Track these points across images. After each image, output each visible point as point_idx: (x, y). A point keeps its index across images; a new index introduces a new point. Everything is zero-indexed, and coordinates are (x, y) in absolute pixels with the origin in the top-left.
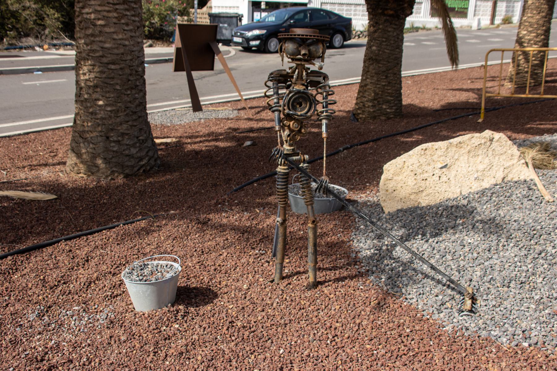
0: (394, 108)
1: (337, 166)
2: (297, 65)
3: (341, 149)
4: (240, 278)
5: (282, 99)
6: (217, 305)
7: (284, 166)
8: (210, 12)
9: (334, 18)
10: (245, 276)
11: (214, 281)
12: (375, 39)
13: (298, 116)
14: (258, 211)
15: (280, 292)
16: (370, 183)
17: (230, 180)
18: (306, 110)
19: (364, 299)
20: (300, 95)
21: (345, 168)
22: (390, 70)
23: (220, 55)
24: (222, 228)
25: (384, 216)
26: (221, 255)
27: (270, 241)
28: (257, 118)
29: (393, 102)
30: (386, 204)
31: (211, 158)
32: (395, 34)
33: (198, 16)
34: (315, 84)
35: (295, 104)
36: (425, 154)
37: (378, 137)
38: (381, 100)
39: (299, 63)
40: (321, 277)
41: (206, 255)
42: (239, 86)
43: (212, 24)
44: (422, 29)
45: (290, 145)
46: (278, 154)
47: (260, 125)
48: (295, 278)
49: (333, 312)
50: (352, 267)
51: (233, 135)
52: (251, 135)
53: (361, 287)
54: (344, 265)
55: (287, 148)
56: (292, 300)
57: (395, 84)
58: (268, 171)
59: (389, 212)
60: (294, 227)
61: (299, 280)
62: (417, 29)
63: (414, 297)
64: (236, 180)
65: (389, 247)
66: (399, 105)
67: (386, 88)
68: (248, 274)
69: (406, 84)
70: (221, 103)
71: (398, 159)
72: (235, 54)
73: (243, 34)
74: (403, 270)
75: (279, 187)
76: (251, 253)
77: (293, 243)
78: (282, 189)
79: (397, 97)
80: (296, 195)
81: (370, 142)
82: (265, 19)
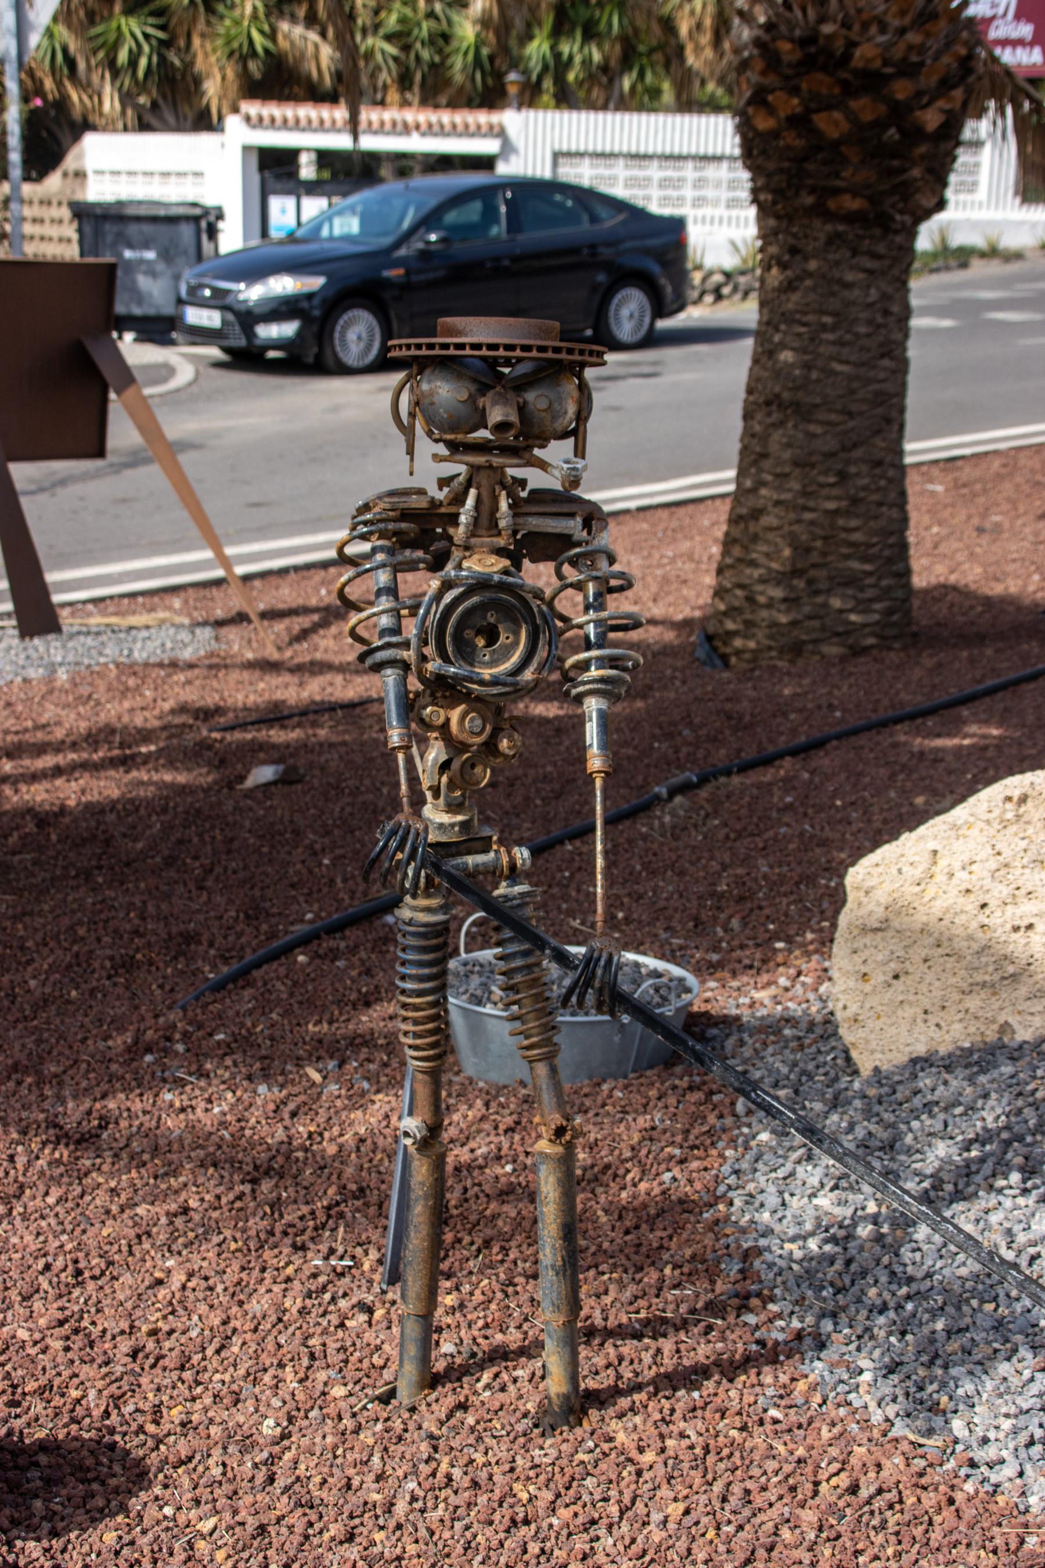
0: (877, 606)
1: (646, 866)
2: (474, 469)
3: (662, 790)
4: (247, 1390)
5: (413, 614)
6: (147, 1522)
7: (428, 896)
8: (79, 197)
9: (611, 221)
10: (267, 1378)
11: (129, 1408)
12: (788, 318)
13: (482, 683)
14: (317, 1077)
15: (425, 1448)
16: (789, 940)
17: (190, 938)
18: (515, 658)
19: (788, 1468)
20: (489, 595)
21: (682, 873)
22: (855, 445)
23: (130, 393)
24: (157, 1154)
25: (856, 1085)
26: (160, 1282)
27: (373, 1210)
28: (298, 660)
29: (869, 581)
30: (861, 1033)
31: (107, 843)
32: (874, 294)
33: (27, 212)
34: (551, 547)
35: (468, 633)
36: (1018, 817)
37: (816, 734)
38: (823, 573)
39: (480, 460)
40: (597, 1365)
41: (91, 1286)
42: (214, 521)
43: (90, 260)
44: (983, 255)
45: (452, 808)
46: (400, 847)
47: (314, 689)
48: (486, 1377)
49: (657, 1536)
50: (731, 1319)
51: (201, 737)
52: (277, 736)
53: (773, 1413)
54: (693, 1311)
55: (437, 817)
56: (475, 1484)
57: (880, 504)
58: (352, 894)
59: (877, 1070)
60: (475, 1138)
61: (503, 1389)
62: (963, 257)
63: (1005, 1453)
64: (219, 941)
65: (885, 1229)
66: (900, 594)
67: (841, 522)
68: (281, 1365)
69: (922, 496)
70: (143, 593)
71: (907, 839)
72: (196, 380)
73: (227, 292)
74: (949, 1333)
75: (409, 985)
76: (290, 1270)
77: (473, 1218)
78: (420, 994)
79: (889, 561)
80: (479, 1002)
81: (780, 756)
82: (318, 228)
